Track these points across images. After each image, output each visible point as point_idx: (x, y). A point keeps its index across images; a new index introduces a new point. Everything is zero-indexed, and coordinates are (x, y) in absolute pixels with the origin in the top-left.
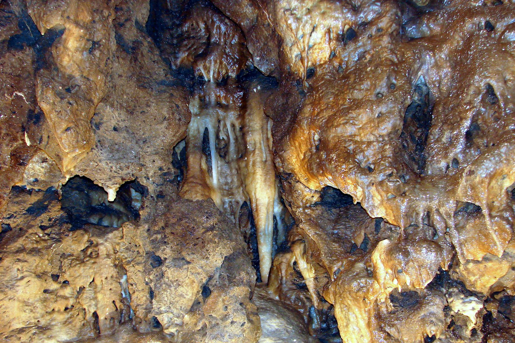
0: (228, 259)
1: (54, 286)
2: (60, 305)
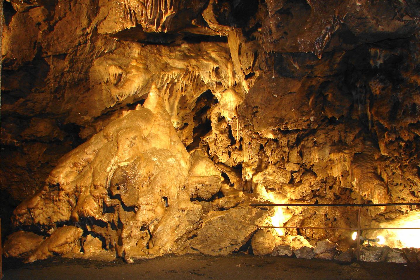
0: (360, 132)
1: (327, 135)
2: (328, 139)
